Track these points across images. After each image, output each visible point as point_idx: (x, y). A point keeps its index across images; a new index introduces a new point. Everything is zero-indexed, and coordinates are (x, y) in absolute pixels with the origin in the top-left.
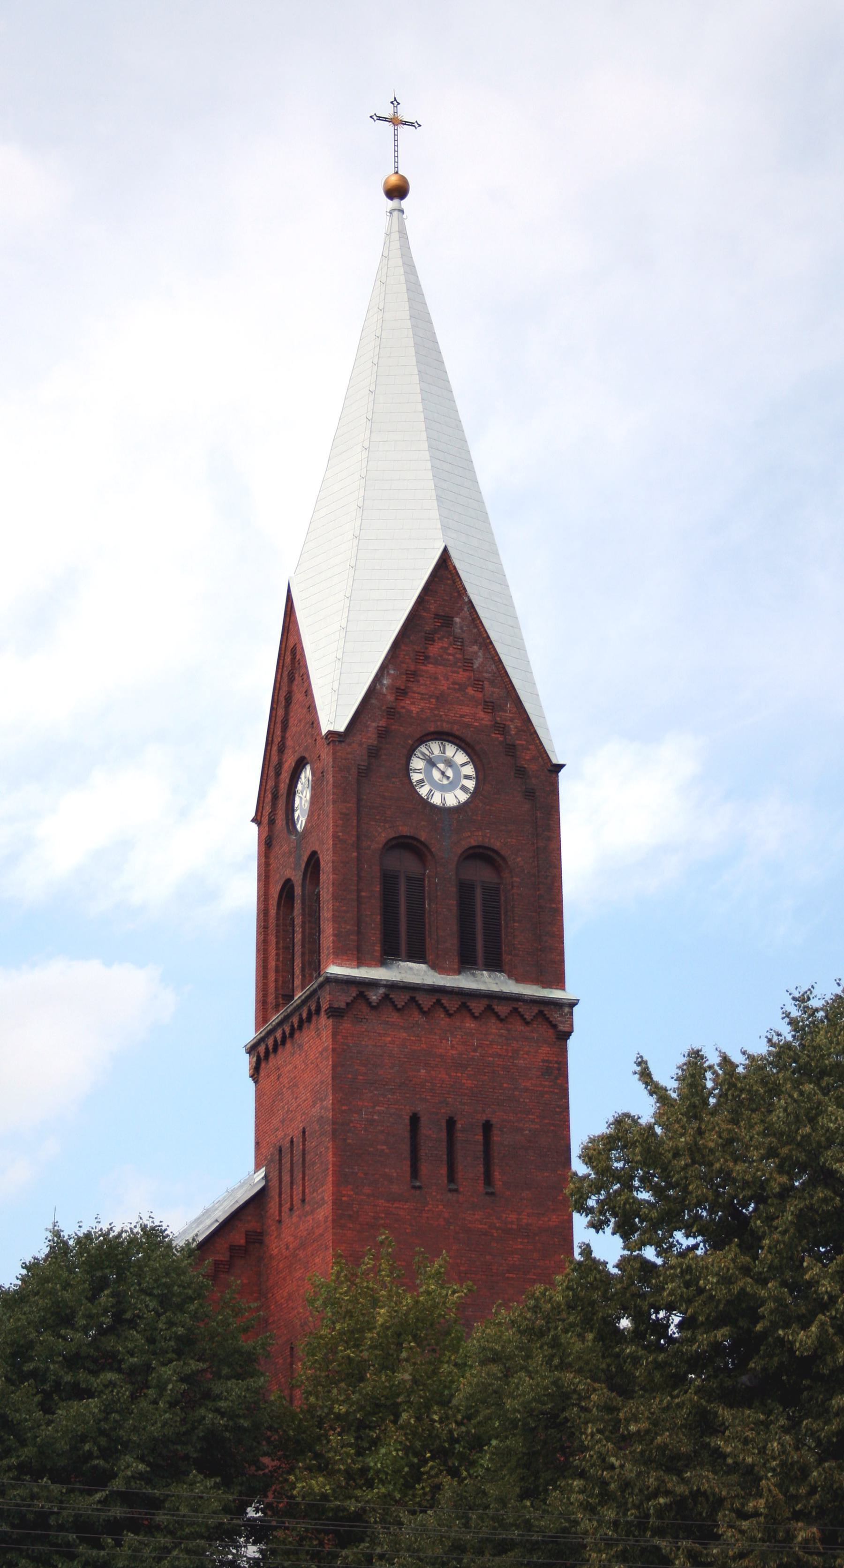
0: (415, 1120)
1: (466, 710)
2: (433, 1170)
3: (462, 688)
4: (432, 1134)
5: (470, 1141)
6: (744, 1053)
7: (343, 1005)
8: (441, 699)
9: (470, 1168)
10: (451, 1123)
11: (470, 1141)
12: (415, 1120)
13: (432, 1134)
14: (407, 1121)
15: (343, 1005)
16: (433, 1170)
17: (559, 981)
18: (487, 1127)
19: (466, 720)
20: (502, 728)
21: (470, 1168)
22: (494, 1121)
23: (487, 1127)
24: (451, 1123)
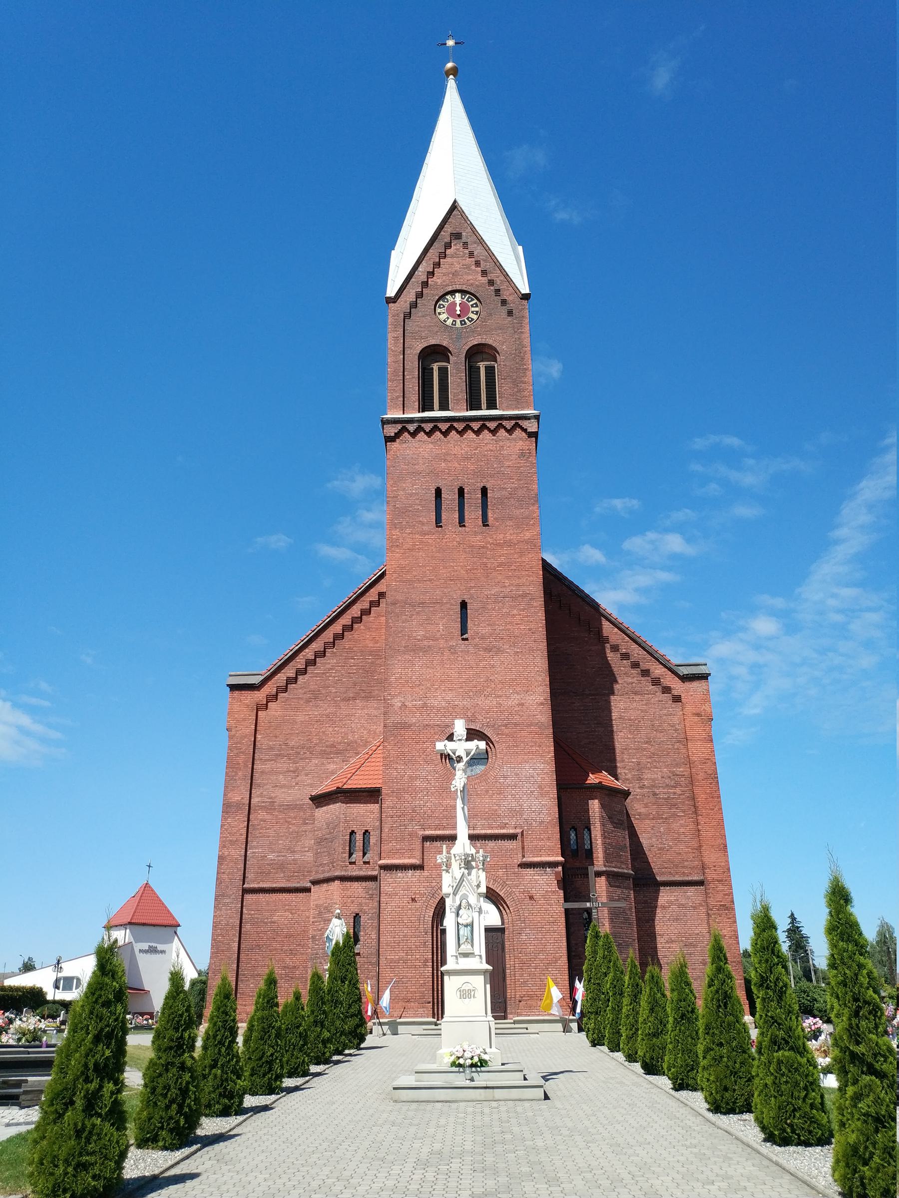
0: (438, 492)
1: (470, 277)
2: (450, 515)
3: (468, 267)
4: (450, 498)
5: (473, 498)
6: (792, 917)
7: (393, 434)
8: (455, 274)
9: (473, 513)
10: (461, 491)
11: (473, 498)
12: (438, 492)
13: (450, 498)
14: (434, 492)
15: (393, 434)
16: (450, 515)
17: (567, 911)
18: (484, 491)
19: (471, 282)
20: (491, 283)
21: (473, 513)
22: (487, 486)
23: (484, 491)
24: (461, 491)
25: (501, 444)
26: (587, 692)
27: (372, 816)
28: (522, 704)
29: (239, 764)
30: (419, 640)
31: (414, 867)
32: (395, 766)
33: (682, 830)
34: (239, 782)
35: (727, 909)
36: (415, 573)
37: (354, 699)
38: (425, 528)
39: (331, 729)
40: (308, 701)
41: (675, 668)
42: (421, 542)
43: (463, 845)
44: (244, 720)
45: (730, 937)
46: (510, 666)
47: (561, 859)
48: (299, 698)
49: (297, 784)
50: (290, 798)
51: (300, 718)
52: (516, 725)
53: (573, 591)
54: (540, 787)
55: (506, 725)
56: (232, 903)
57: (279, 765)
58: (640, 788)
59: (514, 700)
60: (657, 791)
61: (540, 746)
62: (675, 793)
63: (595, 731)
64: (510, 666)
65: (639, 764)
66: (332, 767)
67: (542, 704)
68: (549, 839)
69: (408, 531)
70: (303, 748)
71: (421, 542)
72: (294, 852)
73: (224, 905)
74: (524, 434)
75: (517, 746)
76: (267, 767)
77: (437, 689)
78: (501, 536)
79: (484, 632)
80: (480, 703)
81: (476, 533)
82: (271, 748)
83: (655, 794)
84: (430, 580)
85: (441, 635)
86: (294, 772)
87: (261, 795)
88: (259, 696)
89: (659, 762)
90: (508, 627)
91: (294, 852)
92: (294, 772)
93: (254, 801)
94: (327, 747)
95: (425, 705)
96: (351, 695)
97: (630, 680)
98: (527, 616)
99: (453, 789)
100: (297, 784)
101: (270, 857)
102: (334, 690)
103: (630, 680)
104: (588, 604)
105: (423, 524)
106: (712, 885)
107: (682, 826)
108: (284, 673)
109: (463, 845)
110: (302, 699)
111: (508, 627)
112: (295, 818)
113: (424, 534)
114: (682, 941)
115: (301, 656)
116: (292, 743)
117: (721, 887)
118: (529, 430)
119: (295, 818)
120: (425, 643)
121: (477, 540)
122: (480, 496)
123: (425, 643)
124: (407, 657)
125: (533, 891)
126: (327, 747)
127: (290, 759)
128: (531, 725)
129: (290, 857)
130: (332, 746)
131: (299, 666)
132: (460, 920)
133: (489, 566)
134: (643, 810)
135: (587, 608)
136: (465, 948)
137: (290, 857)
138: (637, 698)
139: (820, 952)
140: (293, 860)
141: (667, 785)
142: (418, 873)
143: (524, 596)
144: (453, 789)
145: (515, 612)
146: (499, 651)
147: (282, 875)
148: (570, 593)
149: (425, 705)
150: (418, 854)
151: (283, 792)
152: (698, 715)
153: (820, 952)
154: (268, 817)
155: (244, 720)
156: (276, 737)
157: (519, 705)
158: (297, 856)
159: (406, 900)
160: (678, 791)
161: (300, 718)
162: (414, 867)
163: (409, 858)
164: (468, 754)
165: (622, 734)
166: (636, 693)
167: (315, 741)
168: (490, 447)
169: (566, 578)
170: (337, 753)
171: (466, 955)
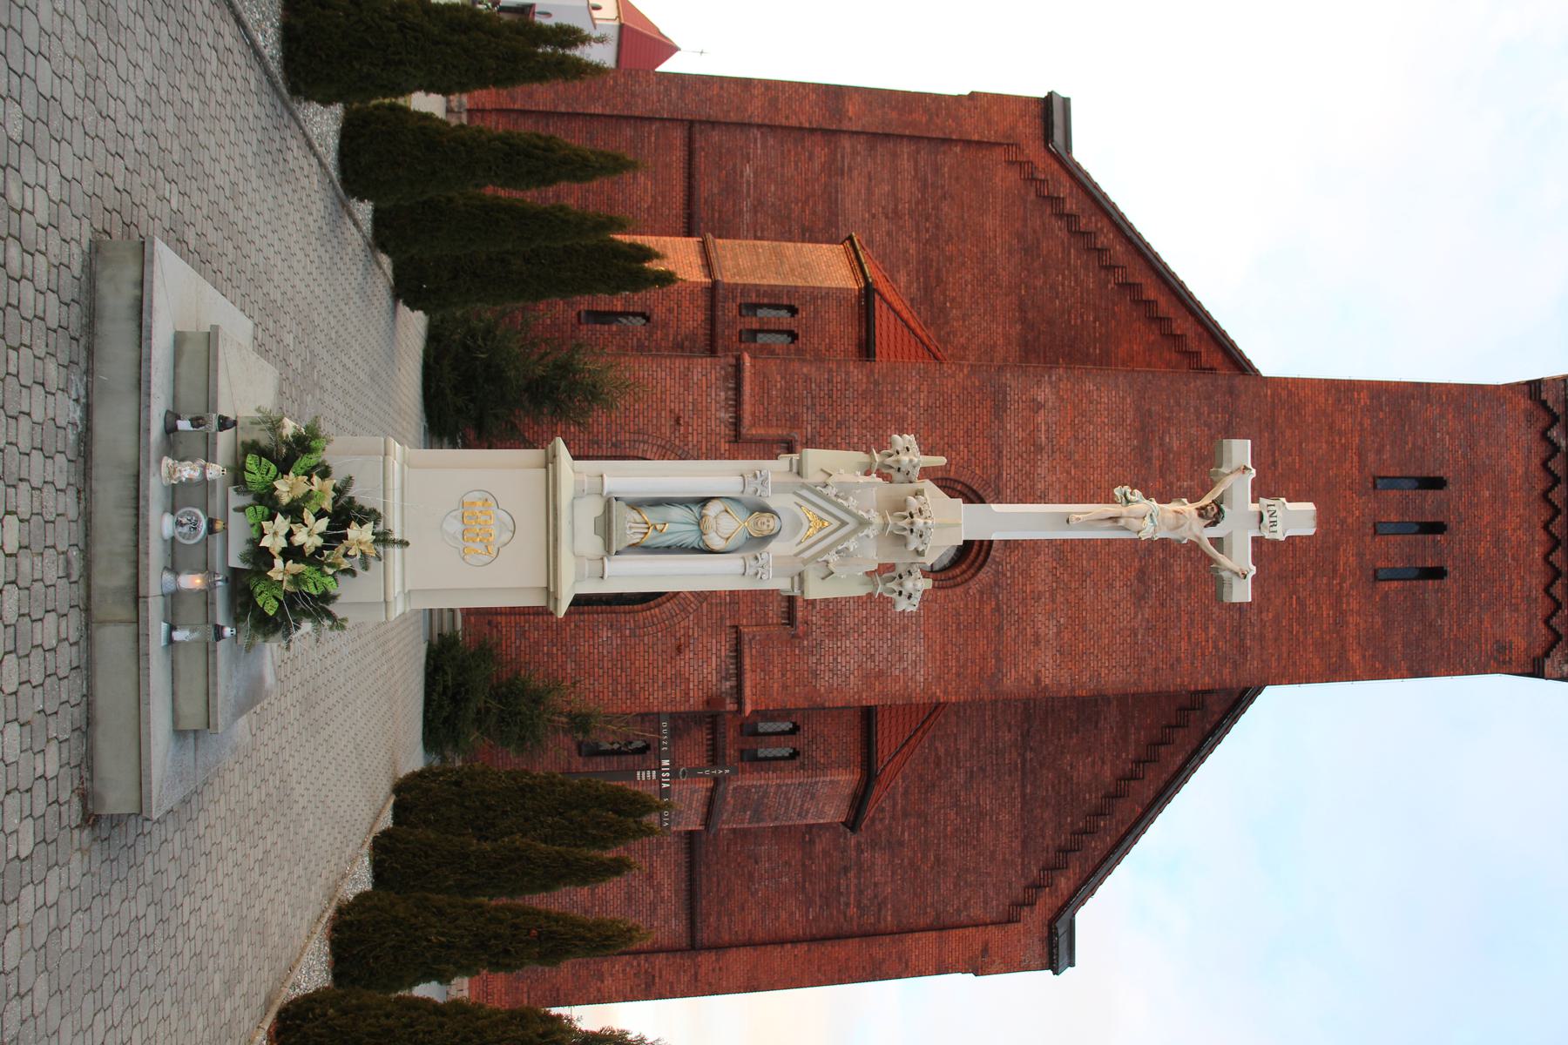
0: (1436, 483)
4: (1429, 505)
5: (1427, 551)
7: (1544, 396)
11: (1427, 551)
12: (1436, 483)
13: (1429, 505)
14: (1437, 474)
15: (1544, 396)
18: (1437, 573)
22: (1447, 581)
23: (1437, 573)
25: (1522, 607)
26: (1029, 755)
27: (822, 348)
28: (1037, 643)
29: (911, 112)
30: (1161, 439)
31: (737, 423)
32: (925, 387)
33: (784, 915)
34: (879, 112)
35: (648, 986)
36: (1288, 433)
37: (1024, 321)
38: (1371, 456)
39: (969, 277)
40: (1020, 237)
41: (1065, 917)
42: (1345, 448)
43: (951, 522)
44: (989, 122)
45: (599, 990)
46: (1109, 619)
47: (748, 709)
48: (1025, 220)
49: (874, 216)
50: (848, 205)
51: (991, 223)
52: (999, 629)
53: (1212, 733)
54: (881, 673)
55: (998, 609)
56: (670, 102)
57: (908, 184)
58: (858, 844)
59: (1048, 629)
60: (851, 874)
61: (958, 675)
62: (847, 905)
63: (958, 767)
64: (1109, 619)
65: (901, 844)
66: (903, 279)
67: (1038, 681)
68: (785, 687)
69: (1366, 422)
70: (937, 227)
71: (1345, 448)
72: (756, 212)
73: (666, 89)
74: (1539, 651)
75: (958, 630)
76: (905, 164)
77: (1069, 473)
78: (1355, 606)
79: (1177, 569)
80: (1042, 558)
81: (1360, 555)
82: (937, 170)
83: (846, 870)
84: (1274, 463)
85: (1171, 484)
86: (895, 211)
87: (855, 153)
88: (1033, 150)
89: (903, 879)
90: (1185, 618)
91: (756, 212)
92: (895, 211)
93: (846, 143)
94: (938, 270)
95: (1040, 449)
96: (1030, 316)
97: (1049, 832)
98: (1203, 654)
99: (1118, 491)
100: (874, 216)
101: (748, 170)
102: (1039, 283)
103: (1049, 832)
104: (1188, 760)
105: (1379, 451)
106: (688, 963)
107: (792, 914)
108: (1071, 193)
109: (951, 522)
110: (1025, 226)
111: (1185, 618)
112: (814, 213)
113: (1361, 455)
114: (594, 905)
115: (1104, 224)
116: (945, 207)
117: (685, 978)
118: (1548, 662)
119: (814, 213)
120: (1156, 452)
121: (1348, 558)
122: (1429, 564)
123: (1156, 452)
124: (1130, 415)
125: (689, 655)
126: (938, 270)
127: (918, 203)
128: (998, 659)
129: (746, 205)
130: (939, 280)
131: (1083, 221)
132: (713, 509)
133: (1300, 581)
134: (818, 848)
135: (1179, 759)
136: (630, 526)
137: (746, 205)
138: (1016, 844)
139: (569, 900)
140: (741, 210)
141: (861, 892)
142: (725, 430)
143: (1242, 650)
144: (1118, 491)
145: (1213, 631)
146: (1139, 599)
147: (716, 190)
148: (1208, 727)
149: (1040, 449)
150: (759, 431)
151: (859, 192)
152: (985, 951)
153: (569, 900)
154: (817, 165)
155: (989, 122)
156: (957, 179)
157: (1037, 635)
158: (747, 217)
159: (676, 406)
160: (853, 911)
161: (991, 223)
162: (737, 423)
163: (753, 414)
164: (1217, 542)
165: (953, 816)
166: (1024, 843)
167: (949, 248)
168: (1517, 585)
169: (1235, 720)
170: (926, 289)
171: (605, 526)
